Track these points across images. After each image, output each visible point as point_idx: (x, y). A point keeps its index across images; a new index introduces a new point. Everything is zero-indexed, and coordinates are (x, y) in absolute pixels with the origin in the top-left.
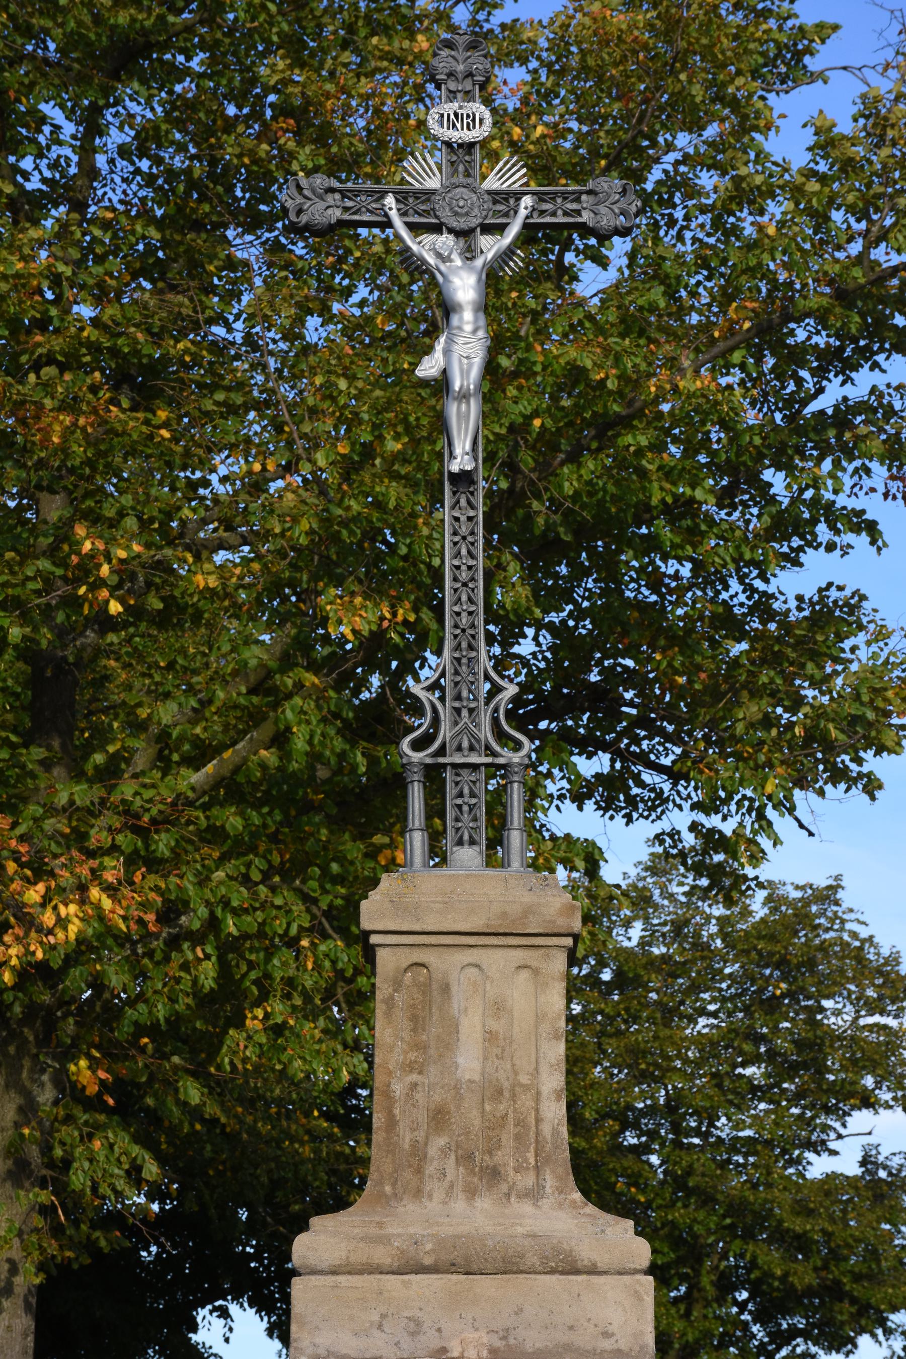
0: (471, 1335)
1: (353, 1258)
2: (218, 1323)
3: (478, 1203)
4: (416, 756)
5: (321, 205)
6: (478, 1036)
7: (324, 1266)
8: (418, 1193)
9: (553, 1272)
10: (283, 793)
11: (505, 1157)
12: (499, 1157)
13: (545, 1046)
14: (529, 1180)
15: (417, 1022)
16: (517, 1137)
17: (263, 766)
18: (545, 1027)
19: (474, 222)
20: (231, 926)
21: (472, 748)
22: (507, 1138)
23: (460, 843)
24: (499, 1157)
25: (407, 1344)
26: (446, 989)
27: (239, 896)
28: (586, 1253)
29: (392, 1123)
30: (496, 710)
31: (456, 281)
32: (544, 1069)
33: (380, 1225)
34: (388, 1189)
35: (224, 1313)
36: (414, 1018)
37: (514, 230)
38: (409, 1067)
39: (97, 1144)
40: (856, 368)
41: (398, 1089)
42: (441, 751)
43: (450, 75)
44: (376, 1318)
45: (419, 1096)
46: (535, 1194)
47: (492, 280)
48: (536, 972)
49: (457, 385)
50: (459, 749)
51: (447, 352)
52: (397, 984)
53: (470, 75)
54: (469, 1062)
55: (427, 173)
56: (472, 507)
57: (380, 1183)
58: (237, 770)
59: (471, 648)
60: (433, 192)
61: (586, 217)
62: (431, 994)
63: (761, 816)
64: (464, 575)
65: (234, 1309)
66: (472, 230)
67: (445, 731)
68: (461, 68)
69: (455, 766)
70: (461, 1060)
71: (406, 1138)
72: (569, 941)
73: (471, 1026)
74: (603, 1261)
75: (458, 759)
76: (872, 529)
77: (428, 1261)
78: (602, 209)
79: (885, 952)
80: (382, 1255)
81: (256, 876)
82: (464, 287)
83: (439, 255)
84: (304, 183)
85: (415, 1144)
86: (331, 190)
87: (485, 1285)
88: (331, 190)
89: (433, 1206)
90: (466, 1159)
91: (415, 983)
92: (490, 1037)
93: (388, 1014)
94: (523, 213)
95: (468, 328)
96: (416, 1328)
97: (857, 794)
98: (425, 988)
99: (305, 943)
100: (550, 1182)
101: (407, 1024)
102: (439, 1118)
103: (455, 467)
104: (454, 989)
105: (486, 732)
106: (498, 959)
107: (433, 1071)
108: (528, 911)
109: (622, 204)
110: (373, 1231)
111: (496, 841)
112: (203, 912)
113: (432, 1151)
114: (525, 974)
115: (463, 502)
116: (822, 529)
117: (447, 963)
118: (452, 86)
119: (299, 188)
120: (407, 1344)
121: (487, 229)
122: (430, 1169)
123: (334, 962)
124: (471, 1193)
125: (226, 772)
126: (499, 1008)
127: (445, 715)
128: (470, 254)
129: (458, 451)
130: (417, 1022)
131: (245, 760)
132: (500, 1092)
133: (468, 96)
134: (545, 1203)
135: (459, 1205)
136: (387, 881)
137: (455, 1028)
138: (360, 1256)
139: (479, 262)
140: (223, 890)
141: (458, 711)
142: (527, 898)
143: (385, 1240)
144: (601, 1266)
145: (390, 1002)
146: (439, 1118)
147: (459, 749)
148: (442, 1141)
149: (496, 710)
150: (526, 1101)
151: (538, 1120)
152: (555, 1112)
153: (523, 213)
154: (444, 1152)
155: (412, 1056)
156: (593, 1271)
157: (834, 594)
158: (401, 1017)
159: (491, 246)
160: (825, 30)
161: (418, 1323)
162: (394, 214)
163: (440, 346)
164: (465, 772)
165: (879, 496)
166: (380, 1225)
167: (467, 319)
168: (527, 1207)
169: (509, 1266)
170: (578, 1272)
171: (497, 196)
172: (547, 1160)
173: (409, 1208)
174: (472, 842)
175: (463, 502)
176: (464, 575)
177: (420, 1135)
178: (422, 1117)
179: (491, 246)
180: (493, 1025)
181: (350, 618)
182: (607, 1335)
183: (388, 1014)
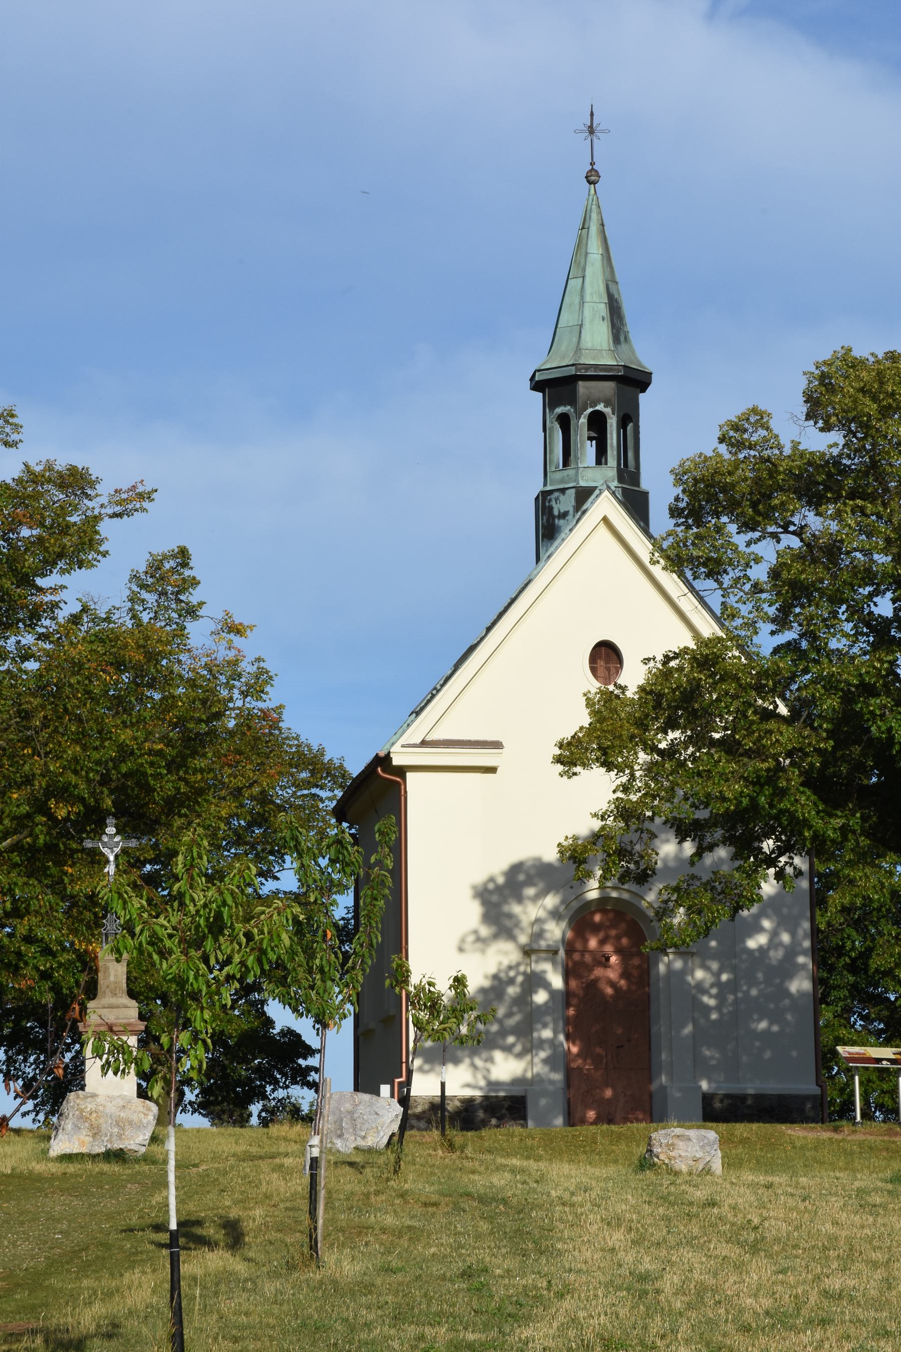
11: (117, 992)
15: (105, 973)
17: (28, 843)
47: (116, 857)
54: (112, 978)
55: (105, 839)
73: (112, 973)
79: (315, 748)
82: (112, 858)
102: (108, 987)
125: (14, 842)
126: (116, 971)
128: (112, 852)
130: (105, 973)
146: (108, 987)
152: (125, 985)
169: (118, 1007)
182: (696, 1160)
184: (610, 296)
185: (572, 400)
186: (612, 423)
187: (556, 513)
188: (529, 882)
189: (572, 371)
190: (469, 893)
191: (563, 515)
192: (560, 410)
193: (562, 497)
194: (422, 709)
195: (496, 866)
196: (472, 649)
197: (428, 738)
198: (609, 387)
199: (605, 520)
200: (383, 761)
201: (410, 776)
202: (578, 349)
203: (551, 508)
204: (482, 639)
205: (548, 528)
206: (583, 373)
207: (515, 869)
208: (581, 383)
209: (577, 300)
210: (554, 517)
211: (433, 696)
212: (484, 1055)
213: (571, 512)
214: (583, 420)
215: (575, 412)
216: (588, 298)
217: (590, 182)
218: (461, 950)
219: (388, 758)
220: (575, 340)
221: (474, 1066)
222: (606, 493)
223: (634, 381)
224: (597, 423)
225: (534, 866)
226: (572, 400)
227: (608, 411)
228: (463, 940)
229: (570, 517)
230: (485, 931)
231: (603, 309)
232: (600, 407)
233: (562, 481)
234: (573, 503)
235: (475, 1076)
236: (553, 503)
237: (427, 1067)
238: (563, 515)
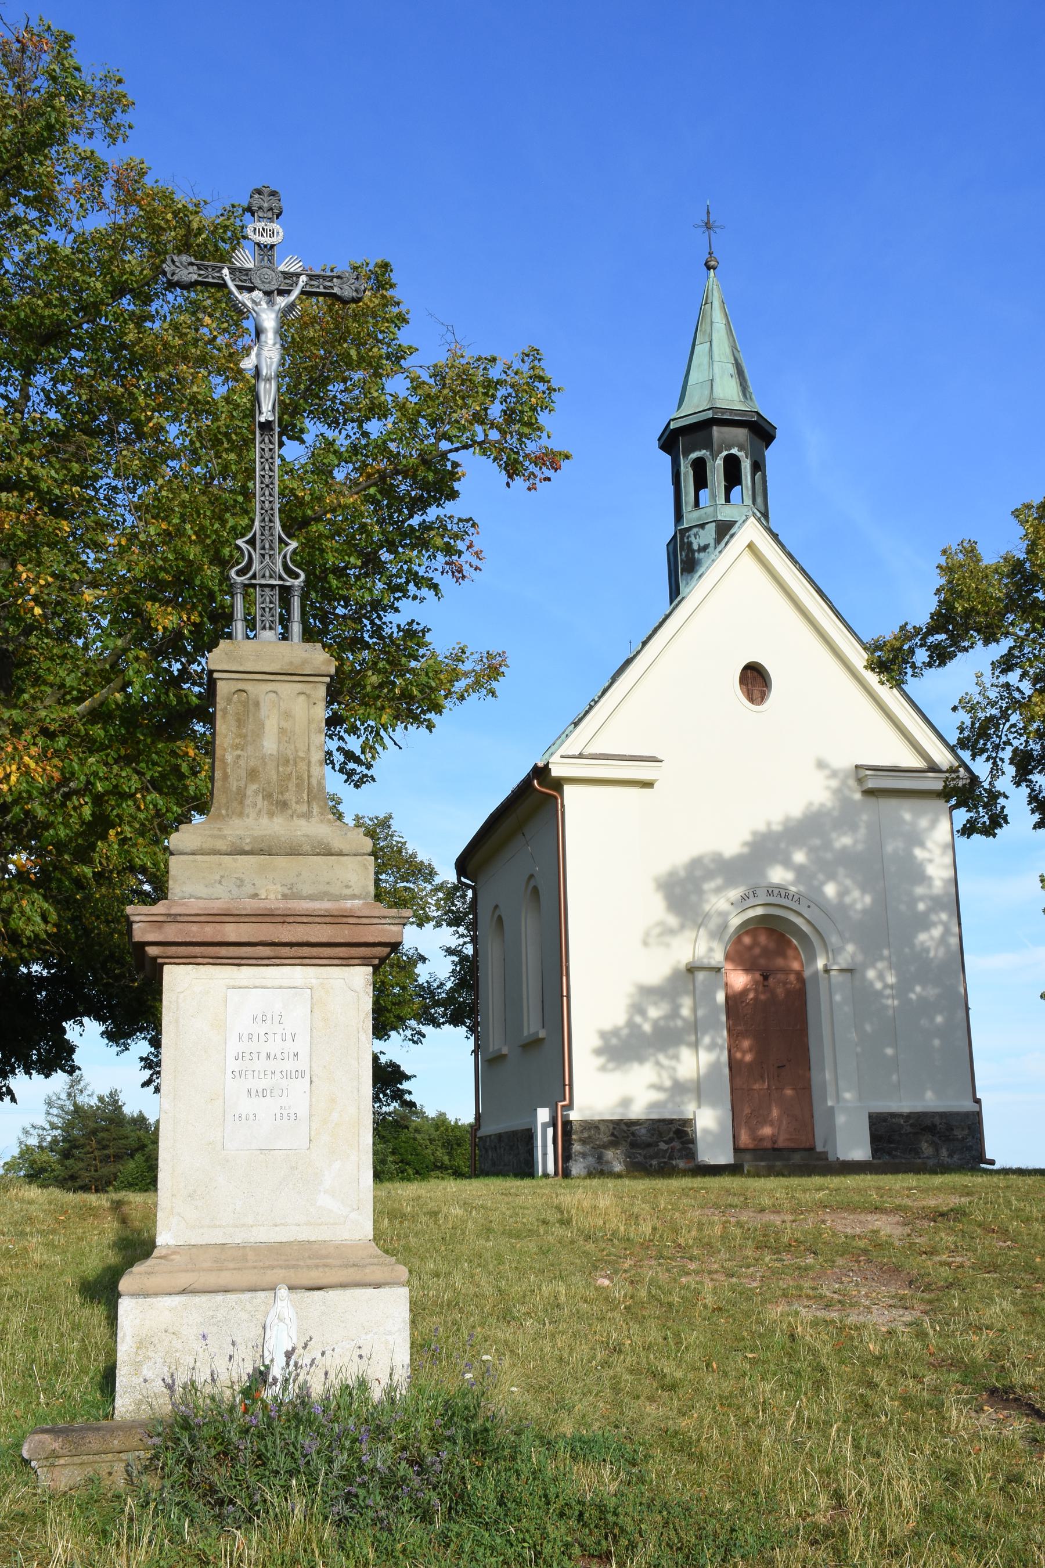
0: (271, 887)
1: (204, 846)
2: (77, 1028)
3: (275, 819)
4: (239, 579)
5: (186, 272)
6: (275, 730)
7: (188, 850)
8: (241, 815)
9: (318, 854)
10: (130, 715)
11: (290, 796)
12: (287, 796)
13: (313, 736)
14: (304, 808)
16: (297, 785)
18: (313, 726)
19: (273, 288)
20: (99, 787)
21: (271, 577)
22: (292, 785)
23: (264, 628)
24: (287, 796)
25: (235, 891)
26: (257, 704)
27: (102, 771)
28: (337, 844)
29: (226, 777)
30: (285, 557)
31: (264, 316)
32: (313, 748)
33: (220, 829)
34: (224, 812)
35: (81, 1024)
36: (239, 720)
37: (296, 292)
38: (236, 747)
39: (24, 903)
40: (430, 505)
41: (229, 758)
42: (254, 577)
43: (260, 208)
44: (218, 878)
45: (242, 762)
46: (307, 816)
48: (308, 696)
49: (264, 372)
50: (264, 576)
51: (258, 355)
52: (229, 701)
53: (271, 209)
54: (270, 744)
55: (246, 258)
56: (271, 442)
57: (219, 809)
58: (102, 704)
59: (270, 521)
60: (250, 270)
61: (336, 290)
62: (249, 707)
63: (378, 734)
64: (267, 480)
65: (86, 1020)
66: (272, 292)
67: (256, 566)
68: (266, 205)
69: (262, 586)
70: (265, 744)
71: (234, 785)
72: (328, 679)
73: (271, 725)
74: (346, 848)
75: (263, 582)
76: (435, 587)
77: (247, 848)
78: (345, 286)
79: (410, 852)
80: (220, 845)
81: (110, 761)
82: (269, 320)
83: (254, 302)
84: (175, 258)
85: (239, 788)
86: (191, 264)
87: (280, 861)
88: (191, 264)
89: (250, 821)
90: (268, 796)
91: (239, 701)
92: (282, 731)
93: (224, 717)
94: (301, 284)
95: (271, 342)
96: (241, 883)
97: (423, 730)
98: (245, 704)
99: (139, 796)
100: (316, 809)
101: (233, 724)
102: (253, 774)
103: (262, 420)
104: (262, 704)
105: (279, 568)
106: (287, 689)
107: (250, 749)
108: (305, 662)
109: (357, 285)
110: (216, 832)
111: (285, 622)
112: (83, 778)
113: (249, 792)
114: (302, 698)
115: (267, 440)
116: (411, 587)
117: (257, 690)
118: (261, 214)
119: (173, 262)
120: (235, 891)
121: (282, 293)
122: (248, 802)
123: (155, 806)
124: (271, 815)
126: (287, 715)
127: (256, 557)
129: (264, 409)
130: (240, 722)
131: (107, 698)
132: (288, 761)
133: (271, 220)
134: (313, 820)
135: (265, 821)
136: (223, 644)
137: (261, 726)
138: (209, 844)
139: (277, 308)
140: (94, 768)
141: (263, 556)
142: (305, 655)
143: (224, 837)
144: (345, 851)
145: (225, 711)
146: (253, 774)
147: (264, 576)
148: (254, 787)
149: (285, 557)
150: (302, 766)
151: (309, 777)
153: (301, 284)
154: (256, 793)
155: (237, 741)
156: (340, 854)
157: (415, 626)
158: (231, 719)
159: (282, 302)
160: (412, 350)
161: (242, 881)
162: (228, 279)
163: (254, 353)
164: (267, 590)
165: (439, 573)
166: (220, 829)
167: (270, 337)
168: (303, 822)
169: (293, 851)
170: (332, 855)
171: (287, 275)
172: (315, 798)
173: (236, 822)
174: (271, 628)
175: (267, 440)
176: (267, 480)
177: (242, 784)
178: (243, 774)
179: (282, 302)
180: (283, 724)
181: (166, 619)
182: (347, 887)
183: (224, 717)
184: (736, 359)
185: (708, 444)
186: (746, 466)
187: (695, 547)
188: (709, 875)
189: (709, 414)
190: (651, 886)
191: (704, 548)
192: (694, 455)
193: (701, 532)
194: (581, 720)
195: (677, 856)
196: (628, 662)
197: (586, 752)
198: (742, 433)
199: (751, 546)
200: (541, 772)
201: (567, 789)
202: (711, 398)
203: (690, 544)
204: (638, 652)
205: (683, 562)
206: (719, 416)
207: (696, 863)
208: (715, 429)
209: (705, 360)
210: (693, 551)
211: (591, 707)
212: (671, 1052)
213: (712, 544)
214: (719, 462)
215: (712, 454)
216: (716, 357)
217: (709, 268)
218: (645, 944)
219: (546, 768)
220: (707, 392)
221: (658, 1063)
222: (752, 519)
223: (762, 432)
224: (732, 466)
225: (713, 860)
226: (708, 444)
227: (741, 454)
228: (647, 934)
229: (710, 550)
230: (673, 921)
231: (731, 369)
232: (734, 451)
233: (699, 519)
234: (714, 536)
235: (660, 1076)
236: (692, 539)
237: (611, 1066)
238: (704, 548)
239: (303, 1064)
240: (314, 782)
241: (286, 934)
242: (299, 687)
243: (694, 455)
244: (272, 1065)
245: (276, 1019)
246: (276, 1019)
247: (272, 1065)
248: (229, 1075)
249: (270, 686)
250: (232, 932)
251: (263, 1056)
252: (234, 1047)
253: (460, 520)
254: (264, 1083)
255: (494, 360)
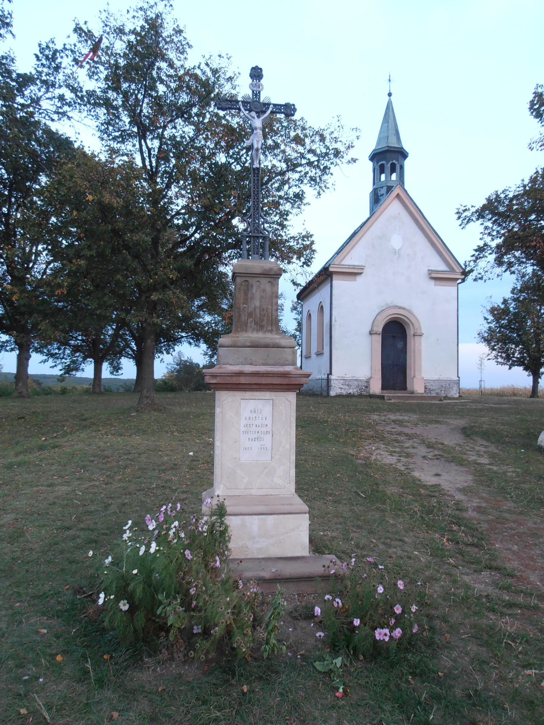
73: (258, 295)
98: (248, 286)
117: (253, 281)
126: (264, 291)
154: (251, 322)
169: (267, 346)
180: (262, 294)
191: (382, 195)
201: (334, 277)
214: (389, 165)
232: (394, 161)
238: (382, 195)
239: (269, 428)
240: (274, 317)
241: (264, 381)
242: (268, 279)
243: (380, 163)
244: (258, 429)
245: (259, 411)
246: (259, 411)
247: (258, 429)
248: (242, 432)
249: (257, 279)
250: (243, 380)
251: (254, 425)
252: (243, 422)
253: (188, 43)
254: (255, 436)
255: (475, 280)
